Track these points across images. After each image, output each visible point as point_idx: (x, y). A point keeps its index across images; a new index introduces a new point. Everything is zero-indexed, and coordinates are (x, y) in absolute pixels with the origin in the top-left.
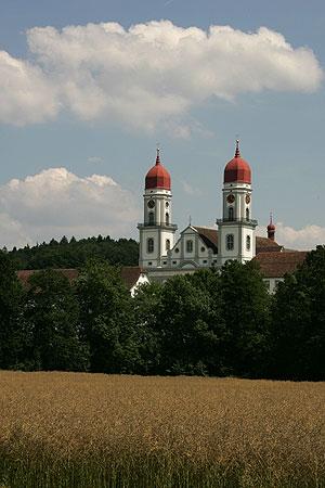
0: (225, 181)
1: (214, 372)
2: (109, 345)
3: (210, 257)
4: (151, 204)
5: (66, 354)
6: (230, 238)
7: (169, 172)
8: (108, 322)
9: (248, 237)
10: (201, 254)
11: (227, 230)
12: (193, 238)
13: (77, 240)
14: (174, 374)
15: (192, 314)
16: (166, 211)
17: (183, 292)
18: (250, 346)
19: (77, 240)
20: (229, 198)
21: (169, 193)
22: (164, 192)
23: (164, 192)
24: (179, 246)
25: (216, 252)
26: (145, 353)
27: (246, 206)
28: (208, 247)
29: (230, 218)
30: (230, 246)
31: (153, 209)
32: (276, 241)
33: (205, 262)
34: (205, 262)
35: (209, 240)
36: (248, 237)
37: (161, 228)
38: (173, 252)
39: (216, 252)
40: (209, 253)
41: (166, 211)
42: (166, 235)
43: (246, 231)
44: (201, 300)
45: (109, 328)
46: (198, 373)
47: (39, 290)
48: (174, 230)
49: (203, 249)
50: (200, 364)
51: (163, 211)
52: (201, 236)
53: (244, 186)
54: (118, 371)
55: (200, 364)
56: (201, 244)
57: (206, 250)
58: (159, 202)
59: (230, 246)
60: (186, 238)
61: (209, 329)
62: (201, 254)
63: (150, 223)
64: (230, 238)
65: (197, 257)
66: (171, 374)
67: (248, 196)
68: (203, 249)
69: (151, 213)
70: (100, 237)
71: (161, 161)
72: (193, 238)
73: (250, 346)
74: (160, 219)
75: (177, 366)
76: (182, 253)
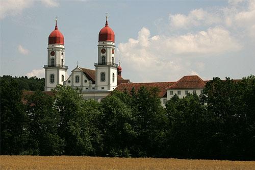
0: (100, 40)
1: (135, 155)
2: (74, 138)
3: (90, 86)
4: (53, 53)
5: (53, 145)
6: (103, 75)
7: (63, 34)
8: (74, 124)
9: (113, 74)
10: (84, 84)
11: (101, 70)
12: (79, 74)
13: (29, 78)
14: (112, 156)
15: (123, 119)
16: (112, 55)
17: (115, 105)
18: (156, 139)
19: (29, 78)
20: (51, 53)
21: (63, 47)
22: (61, 46)
23: (61, 46)
24: (70, 79)
25: (94, 83)
26: (94, 144)
27: (112, 55)
28: (89, 80)
29: (103, 62)
30: (103, 79)
31: (54, 57)
32: (122, 77)
33: (87, 88)
34: (87, 88)
35: (89, 76)
36: (113, 74)
37: (59, 68)
38: (67, 82)
39: (94, 83)
40: (90, 83)
41: (62, 57)
42: (62, 72)
43: (62, 72)
44: (127, 111)
45: (76, 129)
46: (125, 156)
47: (32, 105)
48: (66, 69)
49: (86, 81)
50: (126, 150)
51: (60, 58)
52: (84, 73)
53: (111, 43)
54: (79, 154)
55: (126, 150)
56: (85, 78)
57: (88, 82)
58: (58, 53)
59: (103, 79)
60: (75, 75)
61: (132, 129)
62: (84, 84)
63: (52, 65)
64: (103, 75)
65: (82, 86)
66: (108, 156)
67: (113, 50)
68: (86, 81)
69: (103, 57)
70: (26, 77)
71: (58, 27)
72: (79, 74)
73: (156, 139)
74: (58, 63)
75: (113, 151)
76: (73, 84)
